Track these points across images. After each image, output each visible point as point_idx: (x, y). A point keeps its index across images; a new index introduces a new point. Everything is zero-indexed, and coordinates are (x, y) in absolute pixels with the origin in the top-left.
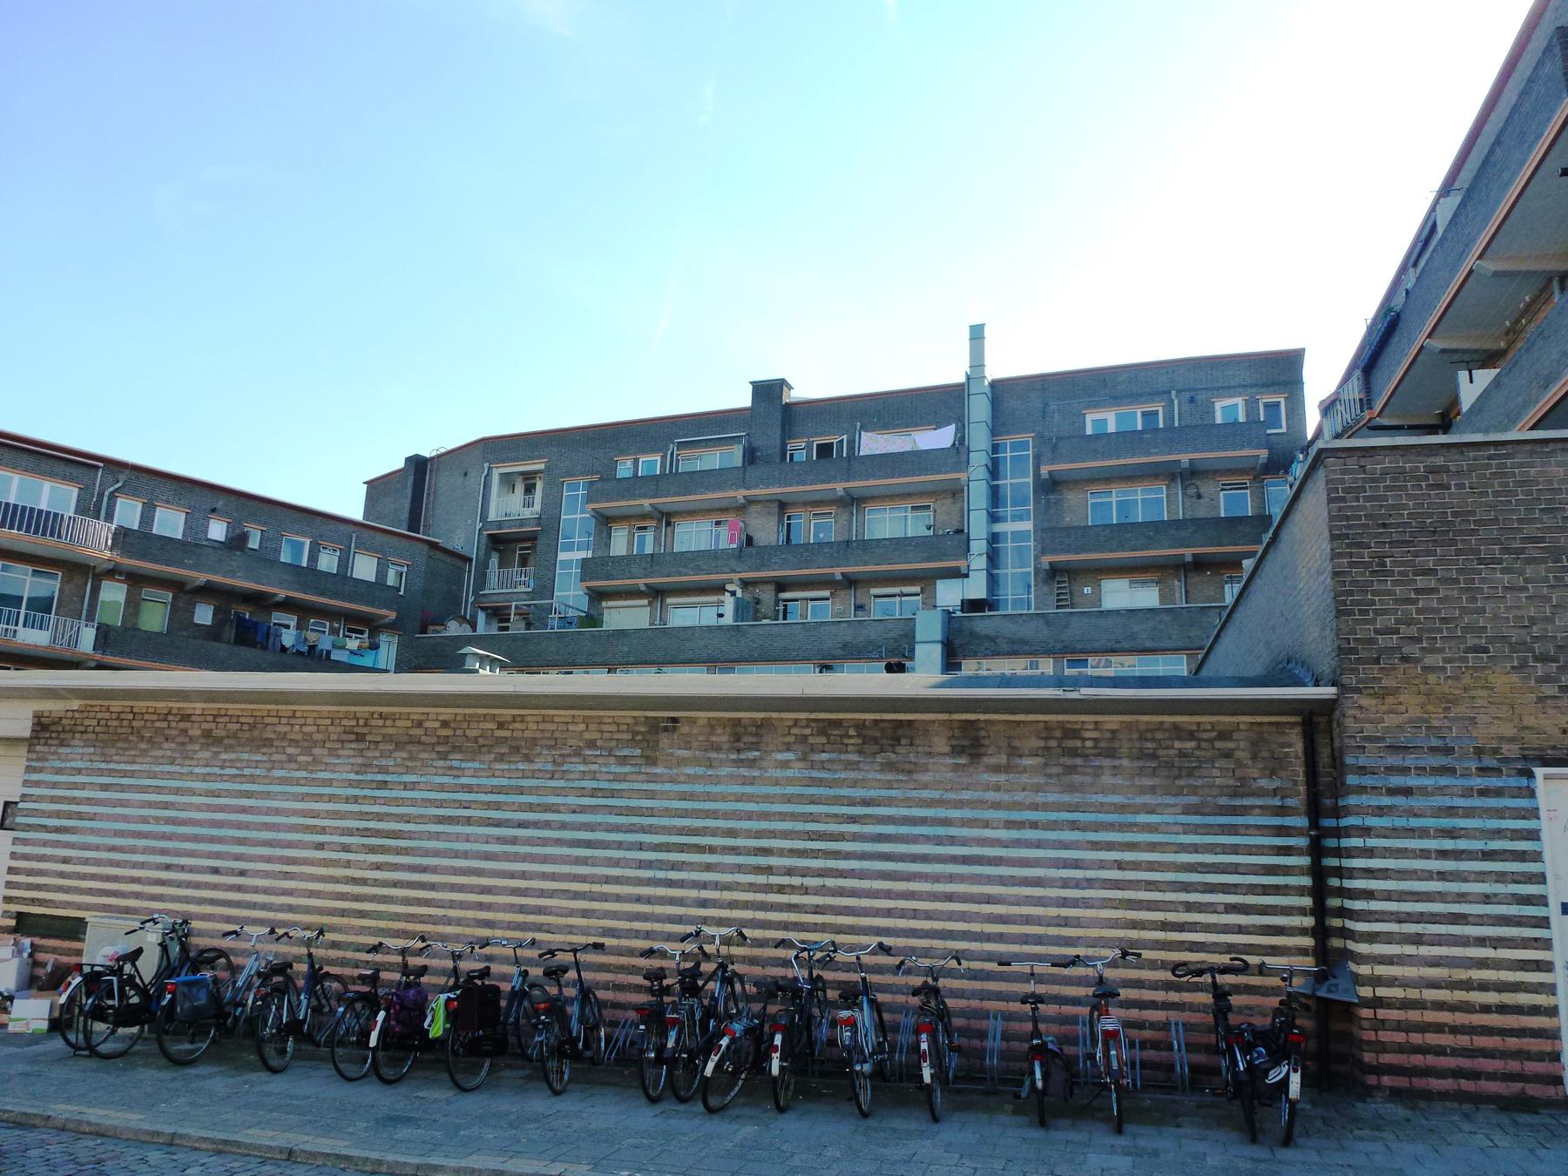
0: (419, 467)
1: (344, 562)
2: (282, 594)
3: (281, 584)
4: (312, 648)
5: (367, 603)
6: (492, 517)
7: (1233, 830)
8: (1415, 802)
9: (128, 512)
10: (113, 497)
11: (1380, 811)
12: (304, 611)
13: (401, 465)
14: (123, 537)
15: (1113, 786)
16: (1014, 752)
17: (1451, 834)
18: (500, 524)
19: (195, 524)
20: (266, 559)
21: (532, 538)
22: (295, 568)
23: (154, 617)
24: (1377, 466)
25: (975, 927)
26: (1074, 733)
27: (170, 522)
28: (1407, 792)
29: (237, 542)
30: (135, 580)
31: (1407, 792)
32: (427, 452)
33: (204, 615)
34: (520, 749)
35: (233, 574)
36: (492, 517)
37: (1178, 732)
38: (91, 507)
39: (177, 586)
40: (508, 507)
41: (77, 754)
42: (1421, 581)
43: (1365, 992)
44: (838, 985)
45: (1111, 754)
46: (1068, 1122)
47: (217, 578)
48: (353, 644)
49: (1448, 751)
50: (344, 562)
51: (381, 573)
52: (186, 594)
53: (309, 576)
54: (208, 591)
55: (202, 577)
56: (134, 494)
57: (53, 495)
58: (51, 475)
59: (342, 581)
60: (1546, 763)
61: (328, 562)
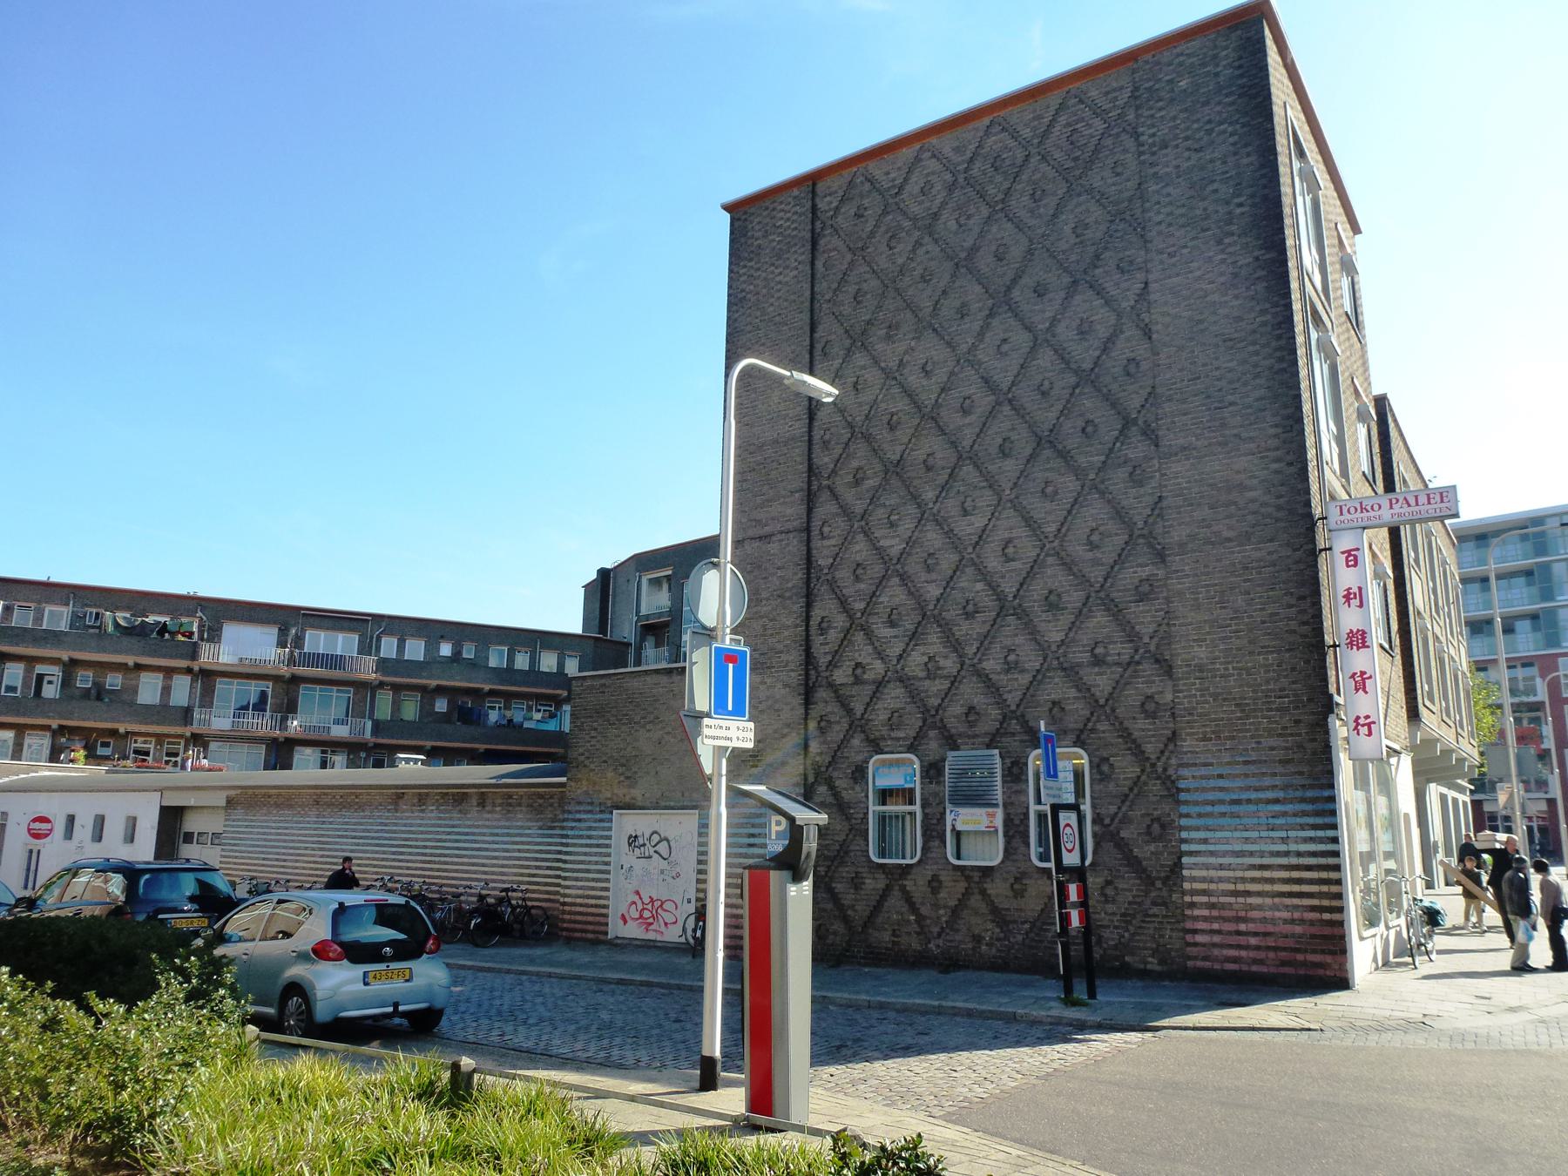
0: (604, 574)
1: (534, 661)
2: (487, 687)
3: (484, 682)
4: (510, 721)
5: (547, 687)
6: (644, 612)
7: (551, 836)
8: (583, 825)
9: (389, 647)
10: (379, 639)
11: (572, 828)
12: (509, 697)
13: (594, 576)
14: (383, 665)
15: (521, 818)
16: (494, 805)
17: (589, 837)
18: (647, 617)
19: (432, 647)
20: (477, 665)
21: (666, 625)
22: (496, 671)
23: (410, 711)
24: (588, 683)
25: (591, 876)
26: (510, 797)
27: (415, 650)
28: (579, 820)
29: (456, 656)
30: (397, 688)
31: (579, 820)
32: (609, 566)
33: (441, 705)
34: (361, 807)
35: (451, 678)
36: (644, 612)
37: (541, 796)
38: (365, 649)
39: (423, 689)
40: (655, 602)
41: (239, 813)
42: (593, 733)
43: (1187, 899)
44: (494, 897)
45: (520, 805)
46: (87, 912)
47: (444, 683)
48: (538, 716)
49: (592, 804)
50: (534, 661)
51: (561, 665)
52: (429, 693)
53: (509, 673)
54: (440, 690)
55: (434, 683)
56: (391, 634)
57: (343, 643)
58: (342, 629)
59: (534, 675)
60: (618, 808)
61: (522, 662)
